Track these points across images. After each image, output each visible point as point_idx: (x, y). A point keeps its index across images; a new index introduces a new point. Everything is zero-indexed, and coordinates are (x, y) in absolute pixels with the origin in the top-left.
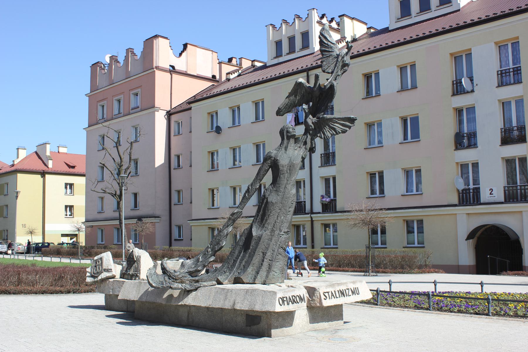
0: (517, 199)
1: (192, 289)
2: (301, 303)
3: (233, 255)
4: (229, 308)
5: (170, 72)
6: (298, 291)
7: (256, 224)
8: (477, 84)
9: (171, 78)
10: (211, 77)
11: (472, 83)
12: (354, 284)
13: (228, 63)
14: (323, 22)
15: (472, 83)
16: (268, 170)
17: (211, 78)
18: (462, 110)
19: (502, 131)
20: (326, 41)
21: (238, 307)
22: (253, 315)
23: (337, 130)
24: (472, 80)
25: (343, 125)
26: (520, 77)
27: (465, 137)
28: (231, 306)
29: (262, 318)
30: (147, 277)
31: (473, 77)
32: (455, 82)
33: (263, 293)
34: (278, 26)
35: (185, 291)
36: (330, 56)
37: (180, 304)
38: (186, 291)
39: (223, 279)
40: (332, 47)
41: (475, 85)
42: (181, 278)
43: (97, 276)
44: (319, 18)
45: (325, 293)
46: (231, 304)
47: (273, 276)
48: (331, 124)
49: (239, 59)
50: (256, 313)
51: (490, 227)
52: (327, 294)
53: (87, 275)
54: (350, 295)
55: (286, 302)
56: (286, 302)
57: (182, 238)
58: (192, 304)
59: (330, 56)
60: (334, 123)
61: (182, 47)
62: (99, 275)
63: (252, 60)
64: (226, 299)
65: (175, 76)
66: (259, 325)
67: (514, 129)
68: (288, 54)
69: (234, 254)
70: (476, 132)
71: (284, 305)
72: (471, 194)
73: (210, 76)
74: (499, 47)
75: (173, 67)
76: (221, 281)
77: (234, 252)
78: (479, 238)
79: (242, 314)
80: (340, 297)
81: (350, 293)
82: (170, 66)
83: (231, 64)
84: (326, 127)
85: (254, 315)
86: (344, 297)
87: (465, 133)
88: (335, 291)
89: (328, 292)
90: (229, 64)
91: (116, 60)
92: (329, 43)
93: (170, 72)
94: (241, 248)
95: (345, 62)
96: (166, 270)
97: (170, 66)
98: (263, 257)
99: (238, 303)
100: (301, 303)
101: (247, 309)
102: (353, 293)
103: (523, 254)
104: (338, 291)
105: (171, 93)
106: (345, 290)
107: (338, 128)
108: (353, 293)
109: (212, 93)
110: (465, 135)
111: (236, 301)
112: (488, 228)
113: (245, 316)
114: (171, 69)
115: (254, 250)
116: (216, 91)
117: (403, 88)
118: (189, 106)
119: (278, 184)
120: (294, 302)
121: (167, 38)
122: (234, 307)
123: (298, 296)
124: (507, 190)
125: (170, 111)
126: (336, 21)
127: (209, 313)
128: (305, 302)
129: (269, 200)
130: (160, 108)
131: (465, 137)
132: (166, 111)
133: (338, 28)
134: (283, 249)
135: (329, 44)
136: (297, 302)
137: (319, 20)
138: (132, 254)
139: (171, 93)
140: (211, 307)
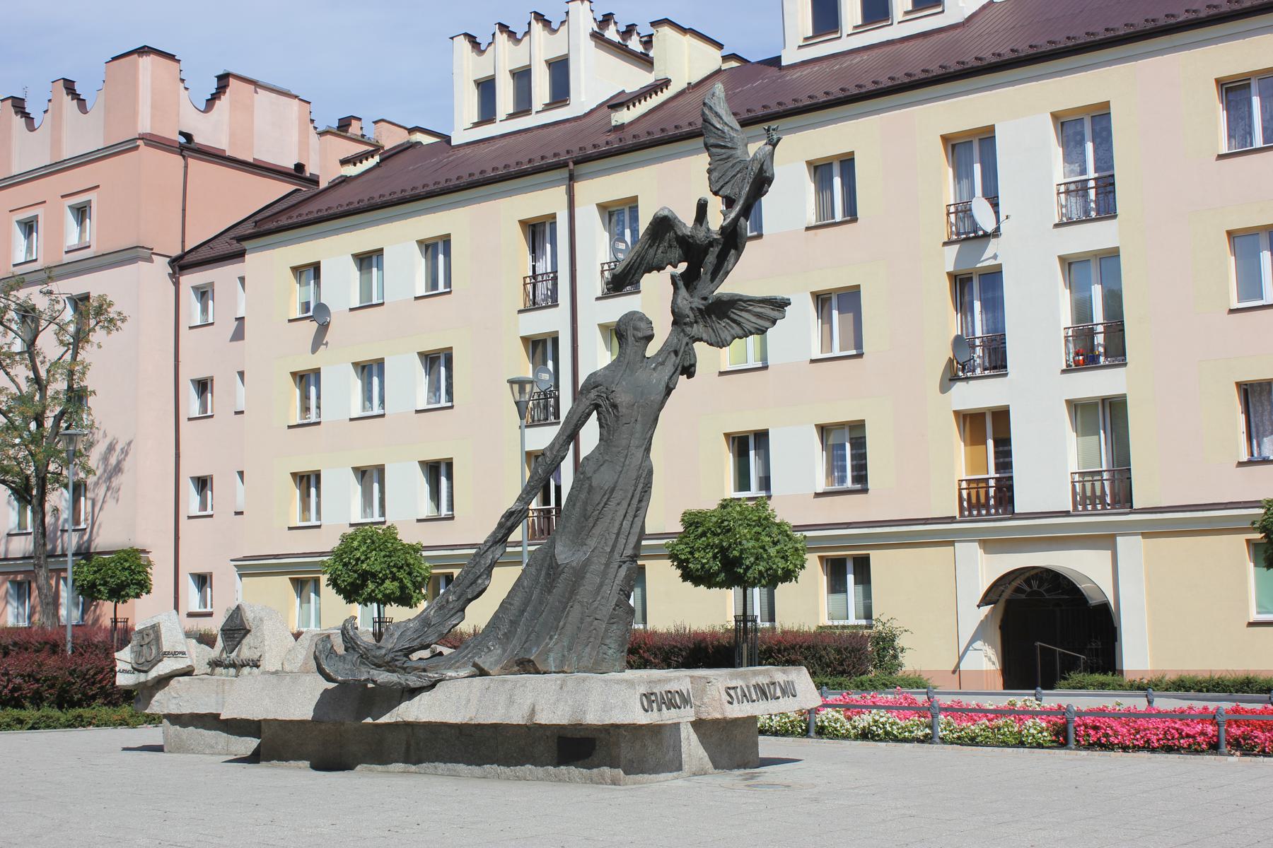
0: (1103, 503)
1: (425, 685)
2: (685, 708)
3: (507, 609)
4: (520, 723)
5: (182, 150)
6: (676, 681)
7: (564, 537)
8: (1007, 216)
9: (186, 167)
10: (293, 167)
11: (995, 212)
12: (784, 673)
13: (339, 132)
14: (630, 47)
15: (997, 213)
16: (589, 415)
17: (293, 172)
18: (970, 279)
19: (1067, 333)
20: (719, 123)
21: (544, 718)
22: (574, 736)
23: (746, 326)
24: (995, 205)
25: (759, 315)
26: (1111, 201)
27: (978, 346)
28: (526, 718)
29: (597, 742)
30: (316, 658)
31: (998, 197)
32: (952, 209)
33: (604, 686)
34: (483, 40)
35: (403, 692)
36: (729, 158)
37: (393, 720)
38: (407, 691)
39: (488, 664)
40: (734, 137)
41: (1002, 217)
42: (390, 662)
43: (145, 669)
44: (597, 25)
45: (729, 688)
46: (526, 710)
47: (604, 655)
48: (733, 312)
49: (374, 122)
50: (582, 733)
51: (1037, 574)
52: (732, 692)
53: (117, 669)
54: (778, 698)
55: (655, 705)
56: (655, 705)
57: (211, 610)
58: (424, 720)
59: (729, 158)
60: (742, 310)
61: (213, 86)
62: (153, 667)
63: (409, 127)
64: (511, 701)
65: (195, 165)
66: (590, 758)
67: (1098, 331)
68: (511, 116)
69: (509, 606)
70: (1005, 335)
71: (652, 711)
72: (1107, 484)
73: (289, 163)
74: (1062, 124)
75: (188, 137)
76: (486, 669)
77: (512, 602)
78: (1009, 603)
79: (547, 736)
80: (758, 701)
81: (779, 693)
82: (181, 133)
83: (348, 135)
84: (710, 317)
85: (578, 737)
86: (767, 700)
87: (978, 338)
88: (748, 687)
89: (734, 688)
90: (342, 133)
91: (22, 110)
92: (726, 129)
93: (182, 150)
94: (526, 592)
95: (764, 174)
96: (356, 643)
97: (181, 133)
98: (582, 613)
99: (542, 710)
100: (685, 708)
101: (565, 722)
102: (784, 692)
103: (1116, 641)
104: (753, 686)
105: (184, 210)
106: (767, 684)
107: (747, 322)
108: (784, 692)
109: (315, 211)
110: (978, 342)
111: (537, 707)
112: (1032, 575)
113: (556, 740)
114: (183, 140)
115: (561, 596)
116: (315, 210)
117: (825, 222)
118: (236, 247)
119: (614, 446)
120: (671, 705)
121: (174, 56)
122: (531, 720)
123: (677, 692)
124: (1079, 482)
125: (181, 257)
126: (638, 34)
127: (463, 740)
128: (691, 707)
129: (594, 483)
130: (152, 249)
131: (978, 346)
132: (168, 259)
133: (643, 52)
134: (625, 594)
135: (726, 131)
136: (677, 705)
137: (596, 29)
138: (238, 614)
139: (184, 210)
140: (475, 724)
